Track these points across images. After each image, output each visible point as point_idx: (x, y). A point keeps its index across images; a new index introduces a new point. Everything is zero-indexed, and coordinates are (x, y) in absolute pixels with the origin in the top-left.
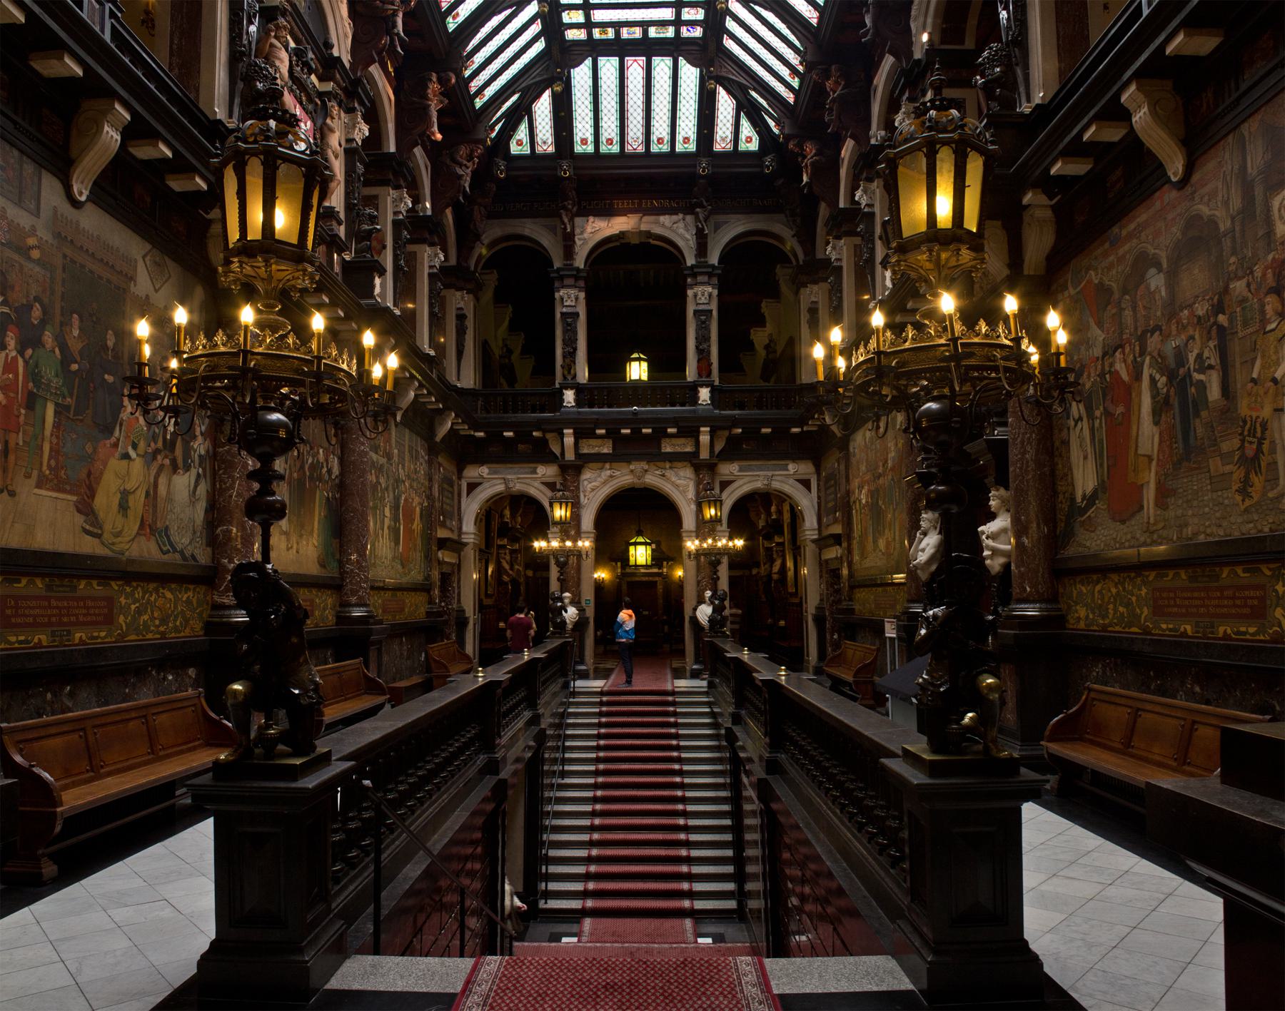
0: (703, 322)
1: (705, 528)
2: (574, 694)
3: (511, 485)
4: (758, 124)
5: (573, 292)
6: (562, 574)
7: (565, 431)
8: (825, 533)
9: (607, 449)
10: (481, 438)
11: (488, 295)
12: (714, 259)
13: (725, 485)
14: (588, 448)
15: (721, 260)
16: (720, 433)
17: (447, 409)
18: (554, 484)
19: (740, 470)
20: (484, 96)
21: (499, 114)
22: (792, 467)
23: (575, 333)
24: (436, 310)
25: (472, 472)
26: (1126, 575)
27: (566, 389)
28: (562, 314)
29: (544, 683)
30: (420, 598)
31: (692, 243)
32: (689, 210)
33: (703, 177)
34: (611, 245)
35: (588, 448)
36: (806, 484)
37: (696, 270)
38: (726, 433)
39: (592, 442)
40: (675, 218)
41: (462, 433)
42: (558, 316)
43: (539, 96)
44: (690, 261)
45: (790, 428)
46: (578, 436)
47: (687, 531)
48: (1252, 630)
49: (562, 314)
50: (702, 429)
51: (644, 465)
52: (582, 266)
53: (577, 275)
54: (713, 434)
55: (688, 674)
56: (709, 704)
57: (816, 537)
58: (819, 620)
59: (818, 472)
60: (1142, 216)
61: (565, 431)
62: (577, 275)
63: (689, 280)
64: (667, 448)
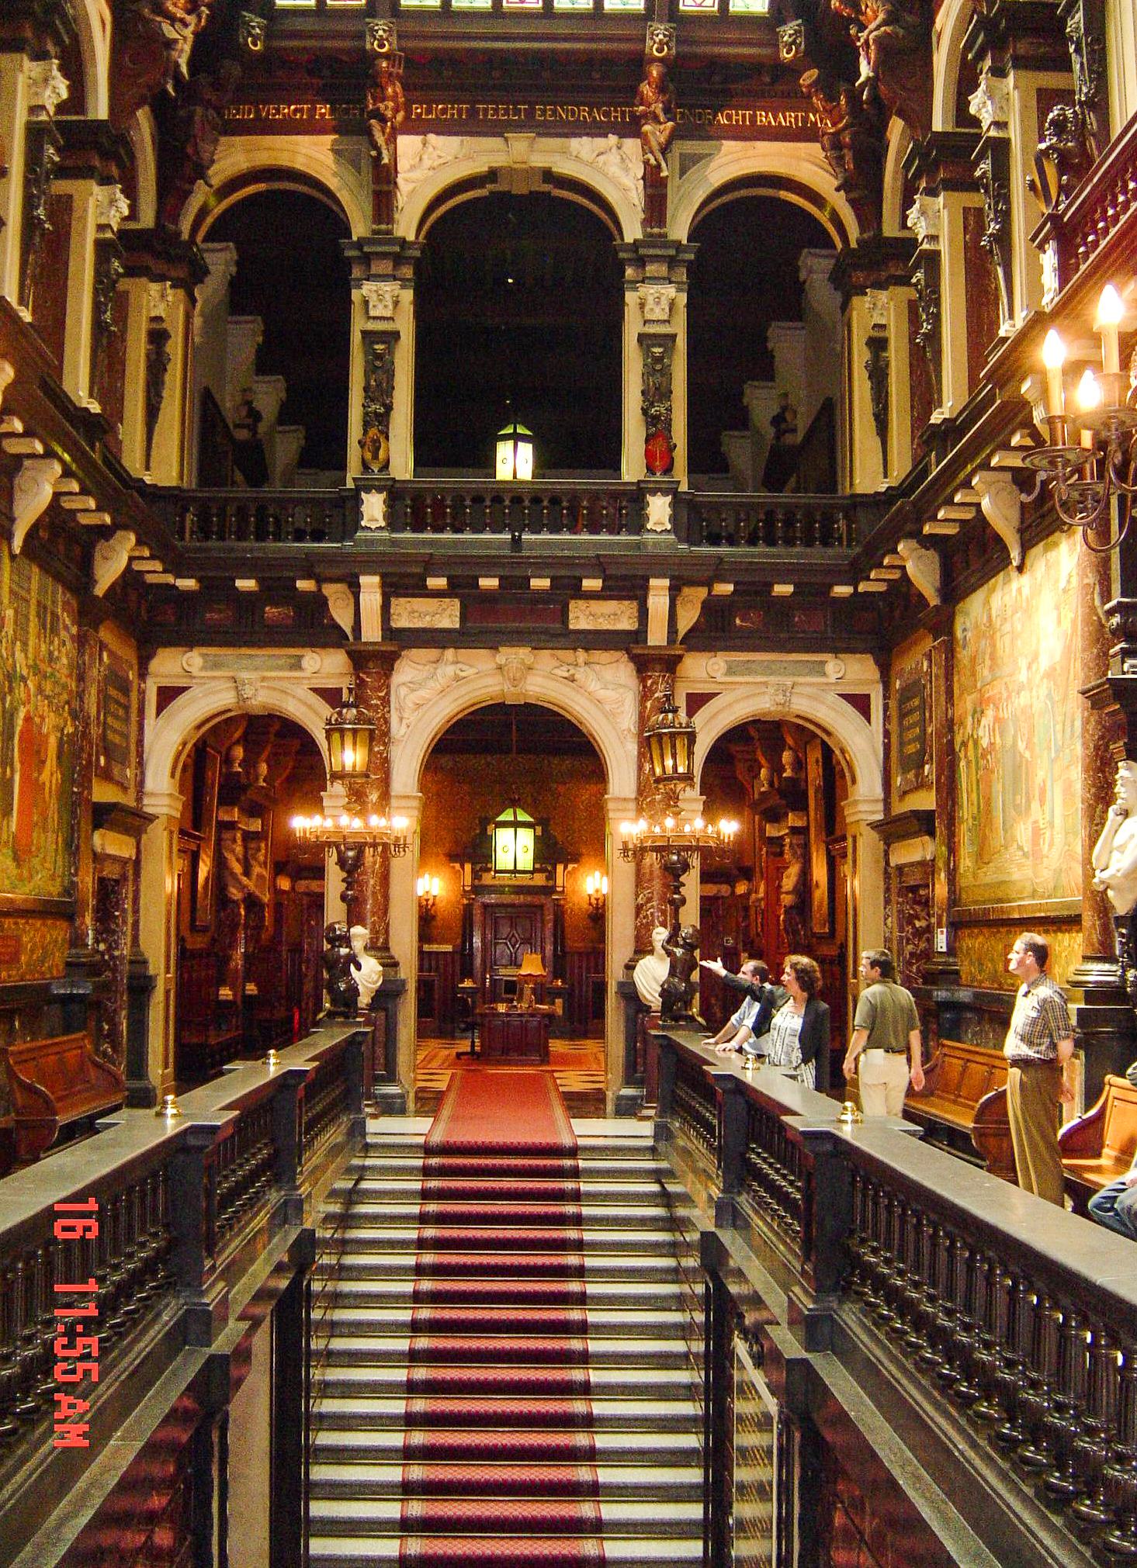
12: (679, 228)
36: (861, 703)
38: (702, 593)
40: (600, 142)
47: (617, 799)
51: (523, 653)
54: (675, 591)
57: (880, 817)
64: (582, 617)
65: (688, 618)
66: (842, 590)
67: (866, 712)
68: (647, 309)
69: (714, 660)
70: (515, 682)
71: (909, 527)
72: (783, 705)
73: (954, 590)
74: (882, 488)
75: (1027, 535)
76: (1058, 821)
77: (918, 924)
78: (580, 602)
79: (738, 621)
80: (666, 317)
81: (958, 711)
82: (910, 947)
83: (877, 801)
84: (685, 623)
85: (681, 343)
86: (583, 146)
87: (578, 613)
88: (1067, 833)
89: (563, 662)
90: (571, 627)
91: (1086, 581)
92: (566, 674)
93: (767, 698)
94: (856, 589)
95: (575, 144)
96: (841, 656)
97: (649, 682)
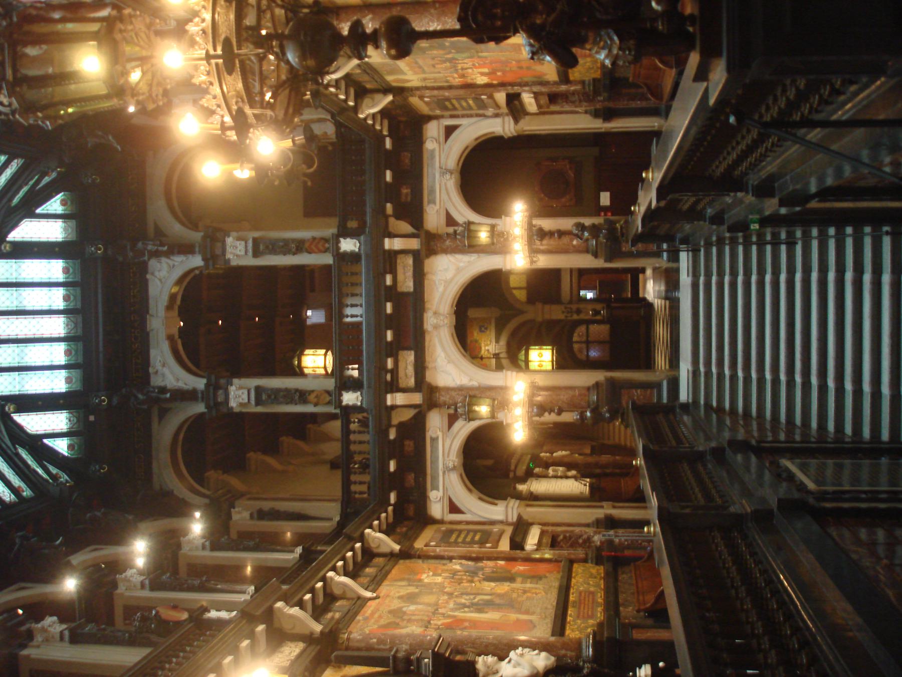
0: (269, 396)
1: (499, 244)
2: (696, 401)
3: (451, 465)
4: (45, 195)
5: (232, 390)
6: (553, 411)
7: (389, 403)
8: (505, 109)
9: (408, 358)
10: (398, 497)
11: (235, 482)
13: (450, 221)
14: (408, 376)
15: (399, 544)
16: (391, 229)
17: (362, 538)
18: (450, 416)
19: (437, 489)
20: (19, 487)
21: (40, 471)
22: (429, 145)
23: (278, 391)
24: (251, 543)
25: (436, 509)
27: (341, 401)
28: (257, 404)
29: (679, 441)
30: (577, 568)
31: (178, 259)
32: (143, 269)
33: (105, 250)
34: (180, 347)
35: (408, 376)
36: (450, 131)
37: (212, 403)
38: (392, 220)
39: (401, 373)
41: (391, 519)
42: (260, 409)
43: (20, 427)
44: (196, 261)
46: (394, 387)
49: (257, 404)
50: (387, 247)
52: (204, 381)
53: (214, 387)
54: (392, 236)
55: (674, 265)
56: (708, 245)
58: (608, 115)
59: (437, 118)
61: (389, 403)
62: (214, 387)
66: (388, 144)
68: (239, 253)
80: (243, 243)
94: (387, 136)
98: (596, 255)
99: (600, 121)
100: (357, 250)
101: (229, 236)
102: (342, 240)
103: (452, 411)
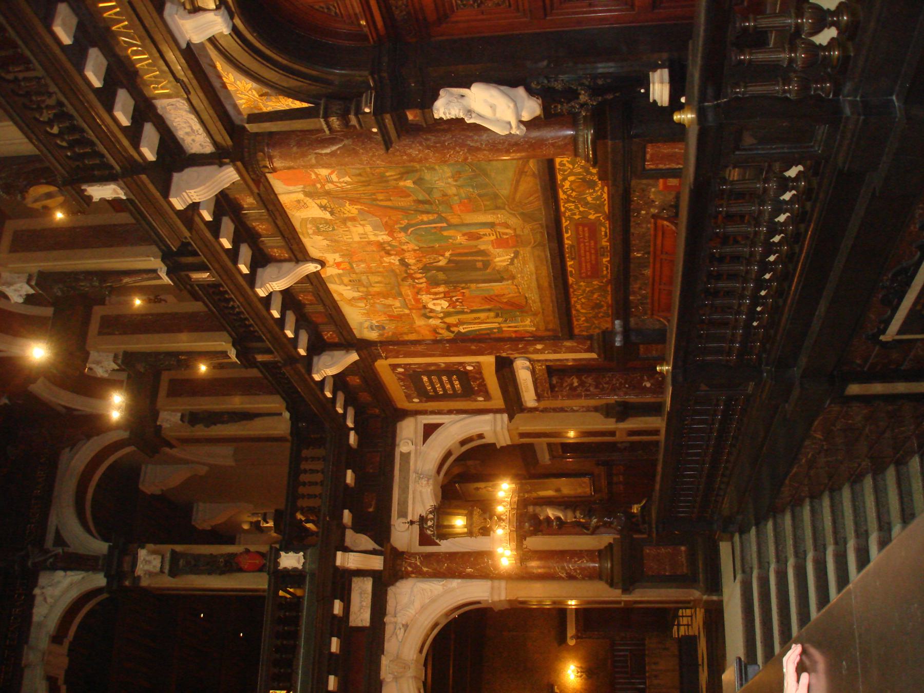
15: (105, 539)
22: (403, 447)
26: (572, 294)
36: (429, 430)
38: (349, 533)
40: (39, 600)
45: (347, 485)
47: (492, 594)
48: (603, 229)
51: (385, 661)
54: (346, 550)
57: (505, 416)
60: (50, 519)
63: (127, 583)
64: (361, 616)
65: (366, 542)
66: (353, 438)
67: (436, 426)
69: (397, 526)
70: (406, 667)
71: (301, 367)
72: (428, 480)
73: (348, 341)
74: (287, 415)
75: (300, 256)
76: (489, 218)
77: (576, 384)
78: (352, 618)
79: (371, 510)
80: (160, 557)
81: (428, 335)
82: (592, 389)
83: (495, 419)
84: (370, 544)
85: (179, 548)
86: (39, 612)
87: (359, 619)
88: (498, 208)
89: (394, 633)
90: (368, 624)
91: (313, 161)
92: (402, 630)
93: (424, 490)
94: (352, 429)
95: (36, 618)
96: (397, 442)
97: (409, 569)
98: (612, 584)
99: (618, 592)
100: (300, 567)
101: (143, 548)
102: (283, 554)
103: (360, 591)
